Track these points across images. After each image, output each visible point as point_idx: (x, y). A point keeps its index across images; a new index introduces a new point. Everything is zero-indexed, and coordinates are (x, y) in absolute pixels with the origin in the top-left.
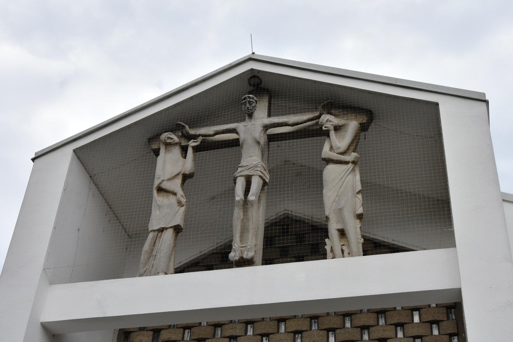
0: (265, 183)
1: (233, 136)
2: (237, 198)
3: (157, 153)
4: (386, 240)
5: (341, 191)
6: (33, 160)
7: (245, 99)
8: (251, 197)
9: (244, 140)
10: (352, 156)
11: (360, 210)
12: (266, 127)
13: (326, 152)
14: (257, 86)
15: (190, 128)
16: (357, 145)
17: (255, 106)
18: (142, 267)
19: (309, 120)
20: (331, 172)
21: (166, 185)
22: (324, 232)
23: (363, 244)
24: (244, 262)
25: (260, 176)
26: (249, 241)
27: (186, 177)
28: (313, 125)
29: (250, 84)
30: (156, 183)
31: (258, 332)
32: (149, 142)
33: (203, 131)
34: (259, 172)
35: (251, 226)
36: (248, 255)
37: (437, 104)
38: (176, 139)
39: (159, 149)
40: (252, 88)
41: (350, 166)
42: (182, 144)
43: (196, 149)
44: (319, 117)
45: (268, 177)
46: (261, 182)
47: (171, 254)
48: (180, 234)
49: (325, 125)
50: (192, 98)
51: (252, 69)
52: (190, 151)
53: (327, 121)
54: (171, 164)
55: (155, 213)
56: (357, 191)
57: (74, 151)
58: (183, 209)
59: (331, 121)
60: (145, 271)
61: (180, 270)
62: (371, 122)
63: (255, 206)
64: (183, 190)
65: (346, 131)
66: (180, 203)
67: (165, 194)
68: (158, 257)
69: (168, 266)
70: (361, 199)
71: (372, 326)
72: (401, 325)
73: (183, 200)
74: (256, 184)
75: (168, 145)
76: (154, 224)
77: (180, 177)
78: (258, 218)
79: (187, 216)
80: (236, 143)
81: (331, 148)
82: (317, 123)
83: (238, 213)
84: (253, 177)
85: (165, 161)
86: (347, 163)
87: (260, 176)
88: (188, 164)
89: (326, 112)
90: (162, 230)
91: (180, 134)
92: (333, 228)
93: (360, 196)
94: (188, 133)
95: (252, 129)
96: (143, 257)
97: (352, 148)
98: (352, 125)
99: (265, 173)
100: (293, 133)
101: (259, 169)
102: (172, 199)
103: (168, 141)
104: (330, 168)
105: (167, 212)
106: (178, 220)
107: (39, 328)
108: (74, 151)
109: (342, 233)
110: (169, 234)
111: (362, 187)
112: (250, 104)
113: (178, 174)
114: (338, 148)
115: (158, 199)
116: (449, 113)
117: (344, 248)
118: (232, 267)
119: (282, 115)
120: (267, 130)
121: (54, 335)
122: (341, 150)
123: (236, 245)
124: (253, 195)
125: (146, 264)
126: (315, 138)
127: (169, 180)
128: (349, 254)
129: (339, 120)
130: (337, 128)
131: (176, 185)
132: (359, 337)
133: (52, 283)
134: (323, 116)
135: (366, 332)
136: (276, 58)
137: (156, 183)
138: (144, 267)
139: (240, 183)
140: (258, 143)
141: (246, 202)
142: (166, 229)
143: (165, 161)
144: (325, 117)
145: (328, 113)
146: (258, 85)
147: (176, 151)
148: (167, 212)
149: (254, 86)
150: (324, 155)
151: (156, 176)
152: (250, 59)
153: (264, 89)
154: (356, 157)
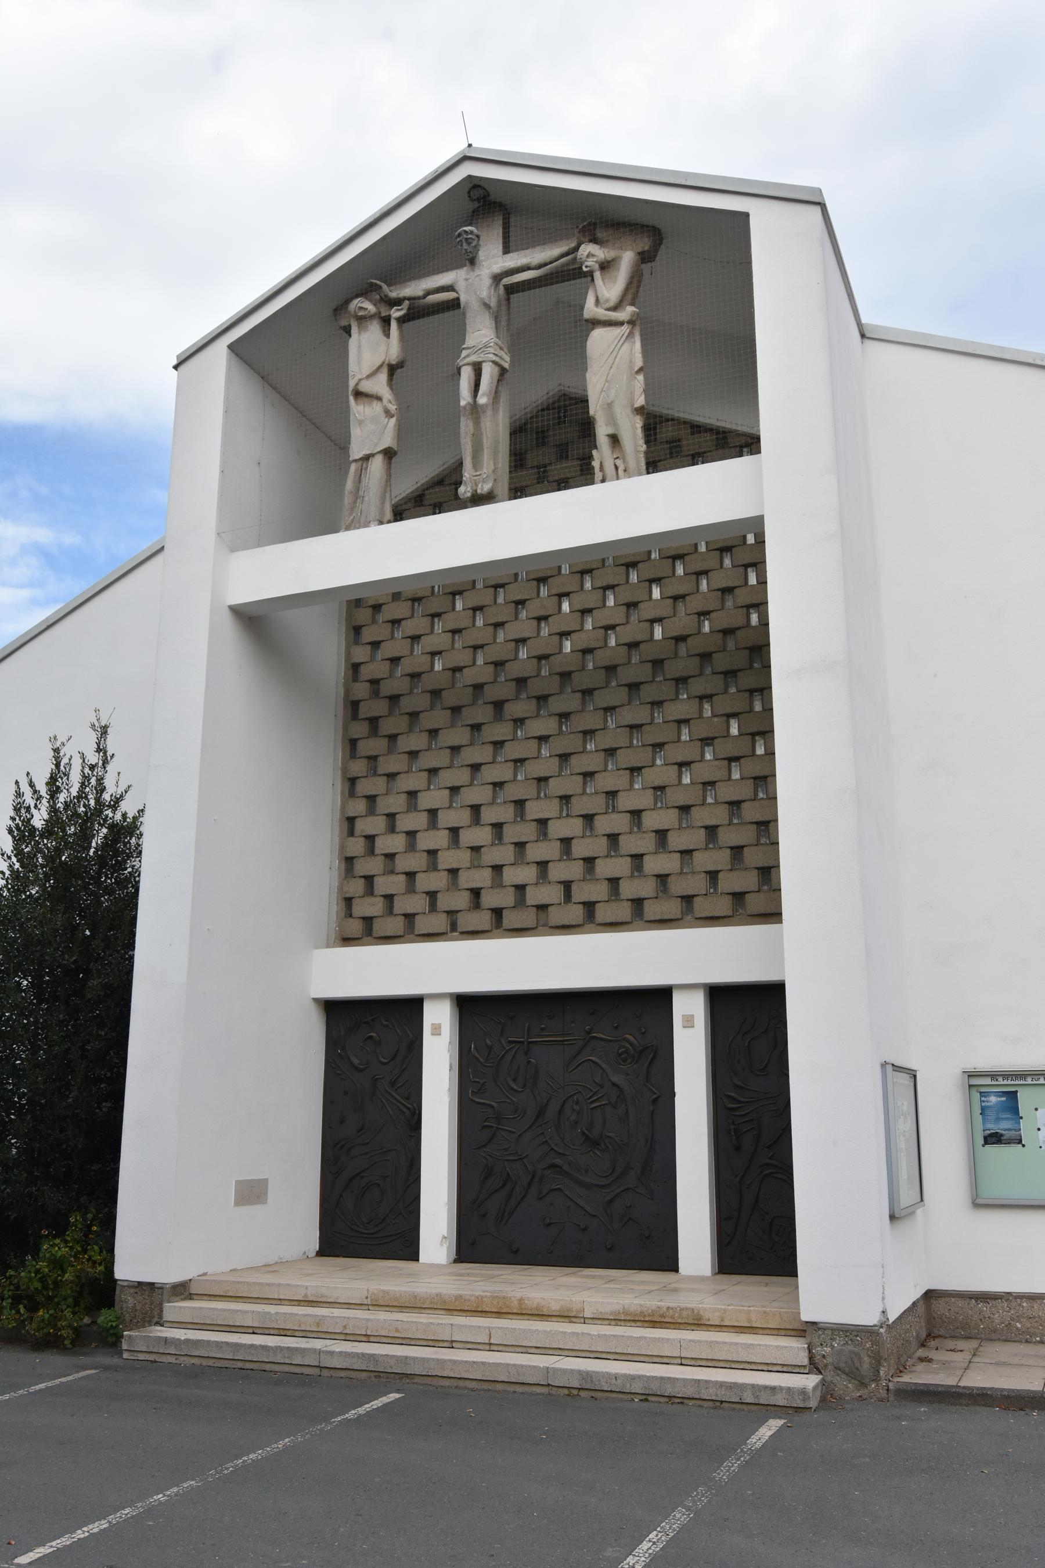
0: (503, 371)
1: (451, 295)
2: (463, 403)
3: (347, 330)
4: (707, 421)
5: (613, 373)
6: (176, 367)
7: (459, 235)
8: (482, 400)
9: (467, 303)
10: (628, 312)
12: (497, 278)
13: (591, 309)
14: (482, 202)
15: (389, 285)
16: (638, 287)
17: (475, 247)
18: (347, 513)
19: (563, 256)
20: (599, 340)
21: (366, 387)
23: (646, 453)
24: (478, 500)
25: (494, 362)
26: (486, 469)
27: (393, 369)
28: (568, 264)
29: (472, 200)
30: (352, 384)
32: (335, 315)
34: (491, 356)
35: (487, 442)
36: (484, 488)
37: (747, 215)
38: (371, 308)
39: (350, 326)
40: (476, 204)
41: (625, 329)
42: (383, 314)
43: (401, 321)
44: (576, 249)
45: (508, 359)
46: (496, 369)
47: (385, 492)
49: (587, 263)
50: (384, 239)
51: (470, 176)
52: (394, 325)
53: (588, 256)
54: (369, 350)
55: (356, 432)
56: (636, 369)
57: (229, 347)
58: (393, 420)
59: (593, 256)
60: (353, 521)
61: (399, 514)
62: (660, 244)
63: (489, 413)
64: (392, 389)
65: (619, 269)
66: (388, 413)
67: (365, 399)
68: (366, 499)
69: (382, 512)
70: (642, 382)
73: (393, 408)
74: (488, 373)
75: (362, 320)
76: (357, 451)
77: (385, 371)
78: (496, 429)
79: (401, 432)
81: (597, 302)
82: (575, 259)
83: (466, 426)
84: (484, 364)
85: (359, 347)
86: (621, 324)
87: (494, 362)
88: (392, 348)
89: (587, 239)
90: (367, 458)
92: (602, 431)
93: (641, 377)
94: (386, 296)
95: (474, 284)
96: (347, 501)
97: (629, 297)
98: (627, 259)
99: (502, 353)
101: (492, 350)
102: (377, 408)
103: (360, 314)
105: (371, 428)
106: (388, 441)
107: (227, 612)
108: (229, 347)
109: (614, 440)
110: (377, 465)
111: (645, 362)
112: (469, 244)
113: (381, 366)
114: (607, 300)
115: (358, 410)
116: (767, 228)
117: (619, 462)
118: (466, 507)
121: (250, 618)
122: (611, 304)
123: (468, 473)
124: (484, 394)
125: (352, 509)
126: (578, 281)
127: (368, 377)
128: (625, 471)
129: (606, 250)
130: (605, 266)
131: (380, 384)
132: (671, 571)
133: (233, 549)
134: (583, 246)
136: (505, 151)
137: (352, 384)
138: (350, 514)
139: (466, 375)
140: (487, 306)
142: (372, 455)
143: (359, 347)
144: (587, 249)
145: (590, 241)
146: (485, 197)
147: (374, 329)
148: (371, 428)
149: (478, 200)
150: (587, 314)
151: (351, 374)
152: (464, 159)
153: (495, 203)
154: (633, 314)
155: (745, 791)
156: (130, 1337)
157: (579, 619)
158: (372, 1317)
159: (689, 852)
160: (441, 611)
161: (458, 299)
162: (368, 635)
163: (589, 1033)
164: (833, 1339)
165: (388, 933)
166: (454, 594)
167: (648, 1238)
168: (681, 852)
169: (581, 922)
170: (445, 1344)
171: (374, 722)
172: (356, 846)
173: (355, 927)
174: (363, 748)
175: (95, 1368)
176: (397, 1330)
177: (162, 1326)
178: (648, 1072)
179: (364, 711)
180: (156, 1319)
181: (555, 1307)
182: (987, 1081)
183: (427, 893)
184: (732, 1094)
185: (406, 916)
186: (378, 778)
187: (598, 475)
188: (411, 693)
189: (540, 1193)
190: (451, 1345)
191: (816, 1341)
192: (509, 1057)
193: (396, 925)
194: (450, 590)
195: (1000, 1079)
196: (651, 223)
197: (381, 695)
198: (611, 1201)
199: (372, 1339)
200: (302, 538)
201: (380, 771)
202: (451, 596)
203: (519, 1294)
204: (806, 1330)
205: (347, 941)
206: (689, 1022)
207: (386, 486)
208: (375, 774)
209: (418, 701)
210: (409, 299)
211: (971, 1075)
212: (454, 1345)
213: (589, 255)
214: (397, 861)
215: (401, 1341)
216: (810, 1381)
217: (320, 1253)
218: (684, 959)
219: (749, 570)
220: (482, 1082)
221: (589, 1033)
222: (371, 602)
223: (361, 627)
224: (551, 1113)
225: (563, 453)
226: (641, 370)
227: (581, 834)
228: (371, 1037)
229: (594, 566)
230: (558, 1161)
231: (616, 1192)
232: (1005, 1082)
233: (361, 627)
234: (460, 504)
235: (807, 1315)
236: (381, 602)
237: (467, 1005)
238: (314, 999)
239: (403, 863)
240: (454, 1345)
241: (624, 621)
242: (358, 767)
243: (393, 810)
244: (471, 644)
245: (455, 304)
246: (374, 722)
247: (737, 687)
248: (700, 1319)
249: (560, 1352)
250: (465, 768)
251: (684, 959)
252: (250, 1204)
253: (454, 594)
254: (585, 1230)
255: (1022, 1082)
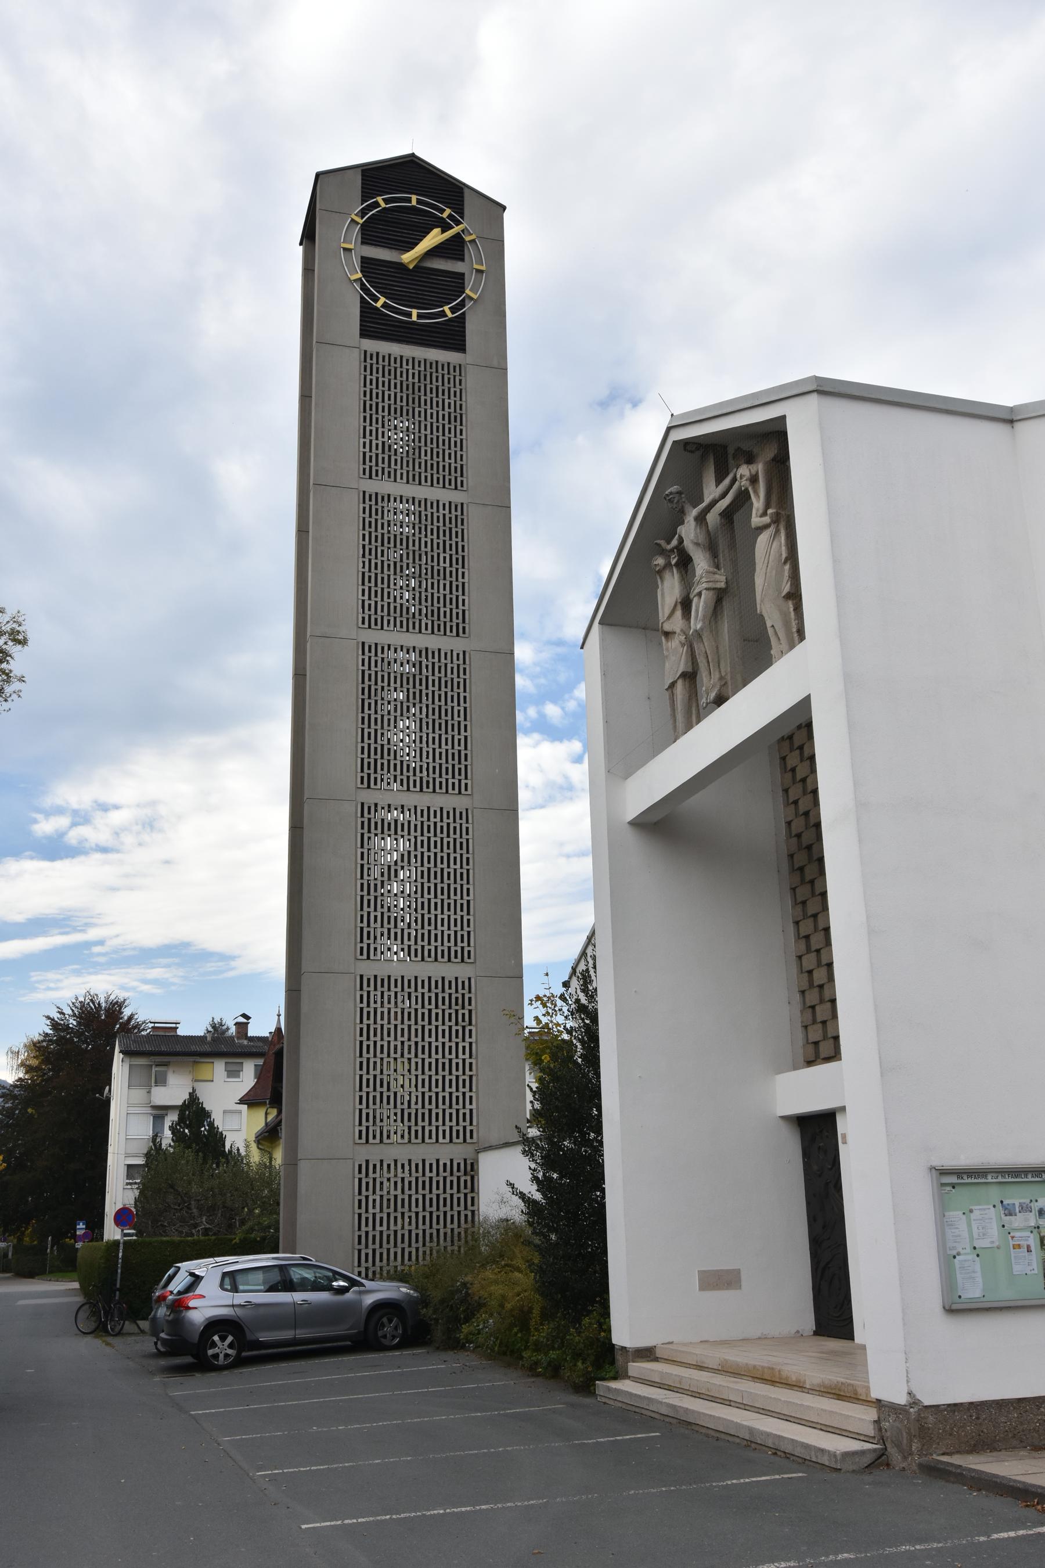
20: (763, 539)
41: (772, 530)
54: (670, 589)
75: (660, 572)
113: (675, 606)
133: (627, 775)
152: (669, 429)
190: (729, 1403)
195: (965, 1177)
205: (810, 1063)
207: (690, 699)
217: (816, 1333)
235: (875, 1394)
238: (783, 1117)
252: (719, 1289)
255: (983, 1180)
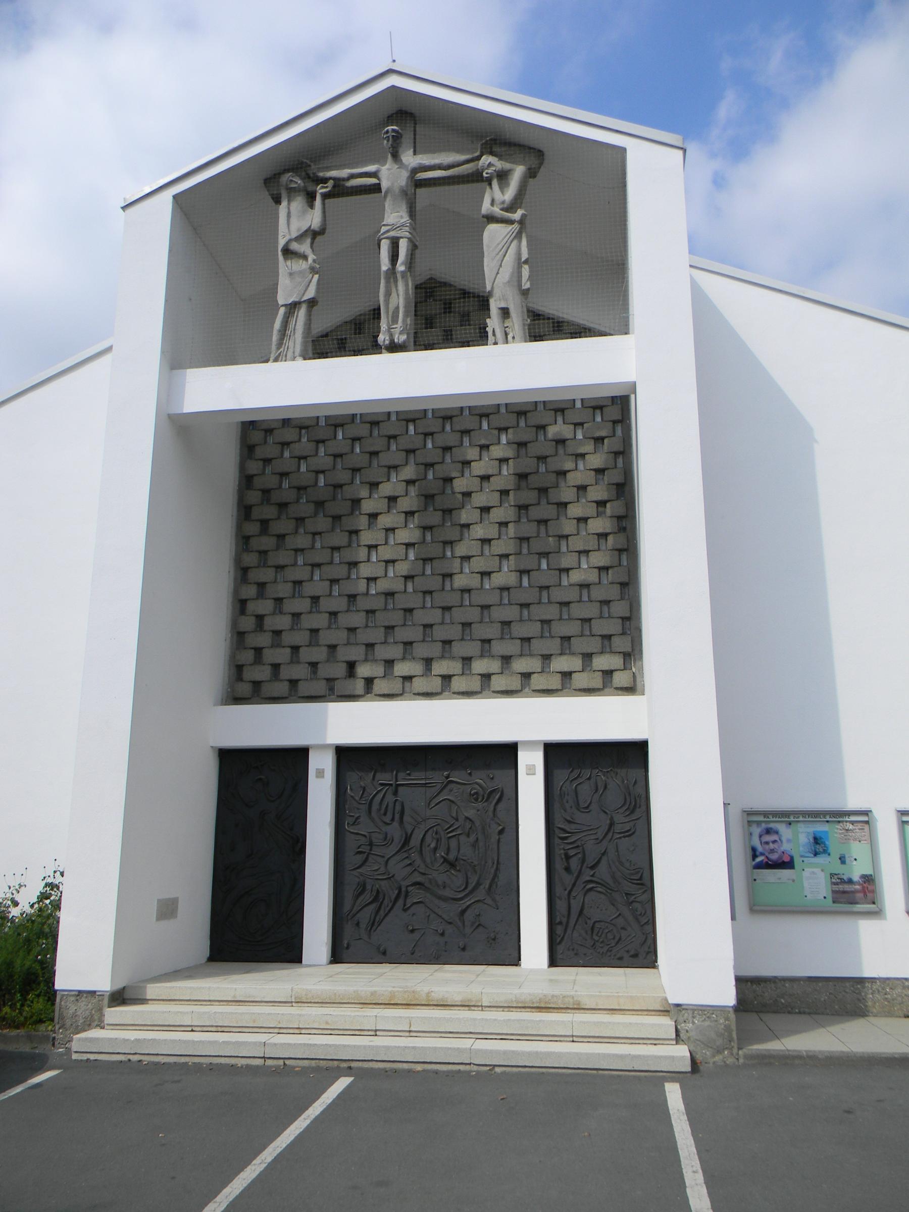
1: (373, 181)
5: (500, 261)
8: (400, 268)
11: (526, 285)
12: (415, 171)
20: (494, 234)
21: (294, 246)
22: (483, 302)
26: (395, 326)
30: (282, 243)
31: (420, 431)
33: (334, 173)
36: (400, 338)
37: (624, 150)
41: (516, 226)
43: (325, 196)
44: (478, 158)
48: (315, 308)
51: (393, 86)
55: (284, 282)
58: (316, 277)
59: (493, 165)
71: (529, 411)
72: (546, 555)
75: (292, 192)
76: (283, 297)
80: (376, 188)
81: (493, 202)
91: (303, 173)
92: (494, 306)
98: (519, 171)
100: (449, 178)
102: (302, 265)
104: (492, 227)
106: (311, 293)
109: (505, 313)
111: (529, 254)
115: (284, 267)
119: (434, 152)
120: (416, 173)
124: (402, 264)
135: (523, 418)
138: (278, 348)
139: (385, 245)
141: (392, 271)
144: (486, 159)
155: (614, 592)
156: (80, 1039)
157: (441, 453)
158: (303, 1013)
159: (528, 640)
160: (325, 438)
161: (379, 184)
162: (260, 452)
163: (447, 777)
164: (694, 1017)
165: (276, 695)
166: (336, 426)
167: (494, 939)
168: (522, 639)
169: (439, 690)
170: (370, 1033)
171: (265, 524)
172: (248, 623)
173: (244, 689)
174: (255, 543)
175: (59, 1069)
176: (327, 1023)
177: (103, 1028)
178: (495, 809)
179: (256, 513)
180: (96, 1023)
181: (458, 999)
182: (761, 818)
183: (309, 663)
184: (562, 826)
185: (291, 681)
186: (269, 569)
187: (491, 338)
188: (298, 501)
189: (405, 905)
190: (375, 1033)
191: (681, 1019)
192: (381, 795)
193: (282, 688)
194: (333, 423)
195: (770, 817)
196: (536, 146)
197: (272, 502)
198: (463, 912)
199: (303, 1031)
200: (205, 366)
201: (270, 563)
202: (333, 428)
203: (426, 989)
204: (675, 1010)
205: (236, 699)
206: (531, 771)
208: (265, 565)
209: (304, 508)
210: (334, 179)
211: (750, 813)
212: (378, 1033)
213: (490, 165)
214: (283, 637)
215: (329, 1032)
216: (683, 1051)
218: (531, 720)
219: (302, 461)
220: (357, 815)
221: (447, 777)
222: (264, 426)
223: (254, 446)
224: (415, 842)
225: (465, 318)
226: (526, 262)
227: (440, 621)
228: (260, 779)
229: (454, 414)
230: (420, 879)
231: (468, 903)
232: (774, 819)
233: (254, 446)
234: (374, 348)
236: (273, 427)
237: (556, 753)
239: (289, 639)
240: (378, 1033)
241: (478, 458)
242: (250, 559)
243: (281, 595)
244: (351, 466)
245: (376, 188)
246: (265, 524)
247: (527, 517)
248: (579, 1004)
249: (471, 1036)
250: (344, 565)
251: (531, 720)
253: (336, 426)
254: (442, 934)
